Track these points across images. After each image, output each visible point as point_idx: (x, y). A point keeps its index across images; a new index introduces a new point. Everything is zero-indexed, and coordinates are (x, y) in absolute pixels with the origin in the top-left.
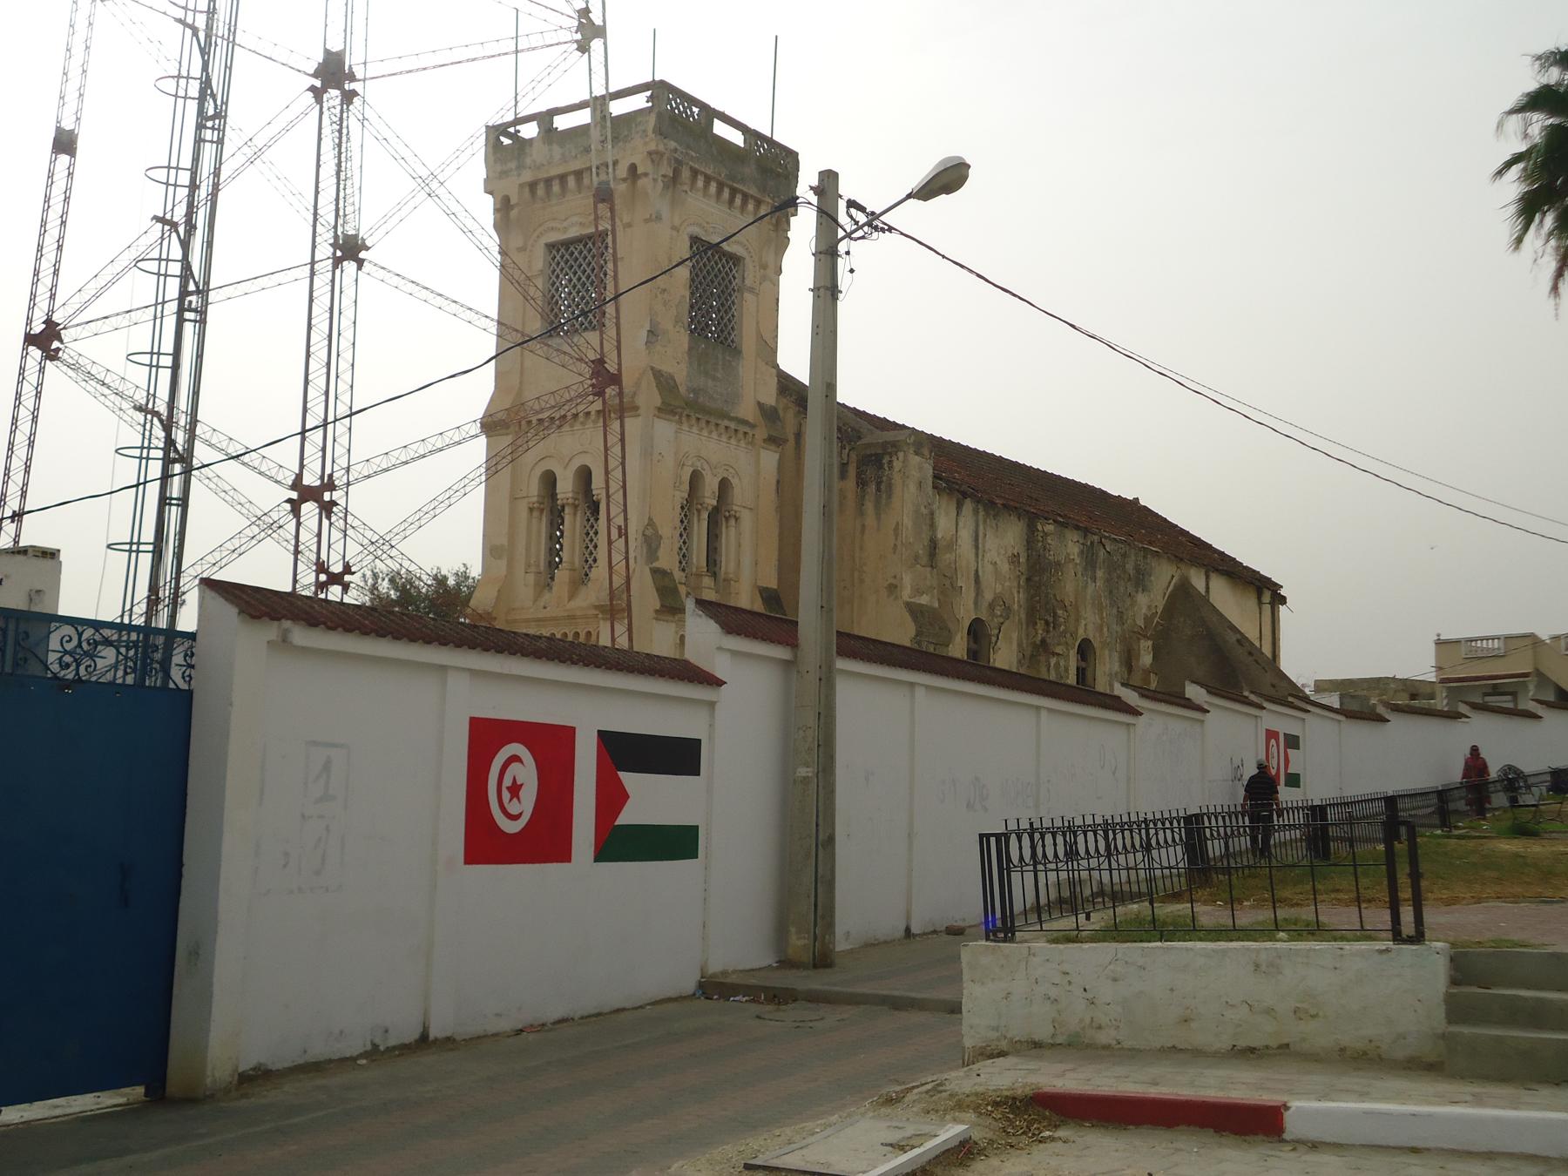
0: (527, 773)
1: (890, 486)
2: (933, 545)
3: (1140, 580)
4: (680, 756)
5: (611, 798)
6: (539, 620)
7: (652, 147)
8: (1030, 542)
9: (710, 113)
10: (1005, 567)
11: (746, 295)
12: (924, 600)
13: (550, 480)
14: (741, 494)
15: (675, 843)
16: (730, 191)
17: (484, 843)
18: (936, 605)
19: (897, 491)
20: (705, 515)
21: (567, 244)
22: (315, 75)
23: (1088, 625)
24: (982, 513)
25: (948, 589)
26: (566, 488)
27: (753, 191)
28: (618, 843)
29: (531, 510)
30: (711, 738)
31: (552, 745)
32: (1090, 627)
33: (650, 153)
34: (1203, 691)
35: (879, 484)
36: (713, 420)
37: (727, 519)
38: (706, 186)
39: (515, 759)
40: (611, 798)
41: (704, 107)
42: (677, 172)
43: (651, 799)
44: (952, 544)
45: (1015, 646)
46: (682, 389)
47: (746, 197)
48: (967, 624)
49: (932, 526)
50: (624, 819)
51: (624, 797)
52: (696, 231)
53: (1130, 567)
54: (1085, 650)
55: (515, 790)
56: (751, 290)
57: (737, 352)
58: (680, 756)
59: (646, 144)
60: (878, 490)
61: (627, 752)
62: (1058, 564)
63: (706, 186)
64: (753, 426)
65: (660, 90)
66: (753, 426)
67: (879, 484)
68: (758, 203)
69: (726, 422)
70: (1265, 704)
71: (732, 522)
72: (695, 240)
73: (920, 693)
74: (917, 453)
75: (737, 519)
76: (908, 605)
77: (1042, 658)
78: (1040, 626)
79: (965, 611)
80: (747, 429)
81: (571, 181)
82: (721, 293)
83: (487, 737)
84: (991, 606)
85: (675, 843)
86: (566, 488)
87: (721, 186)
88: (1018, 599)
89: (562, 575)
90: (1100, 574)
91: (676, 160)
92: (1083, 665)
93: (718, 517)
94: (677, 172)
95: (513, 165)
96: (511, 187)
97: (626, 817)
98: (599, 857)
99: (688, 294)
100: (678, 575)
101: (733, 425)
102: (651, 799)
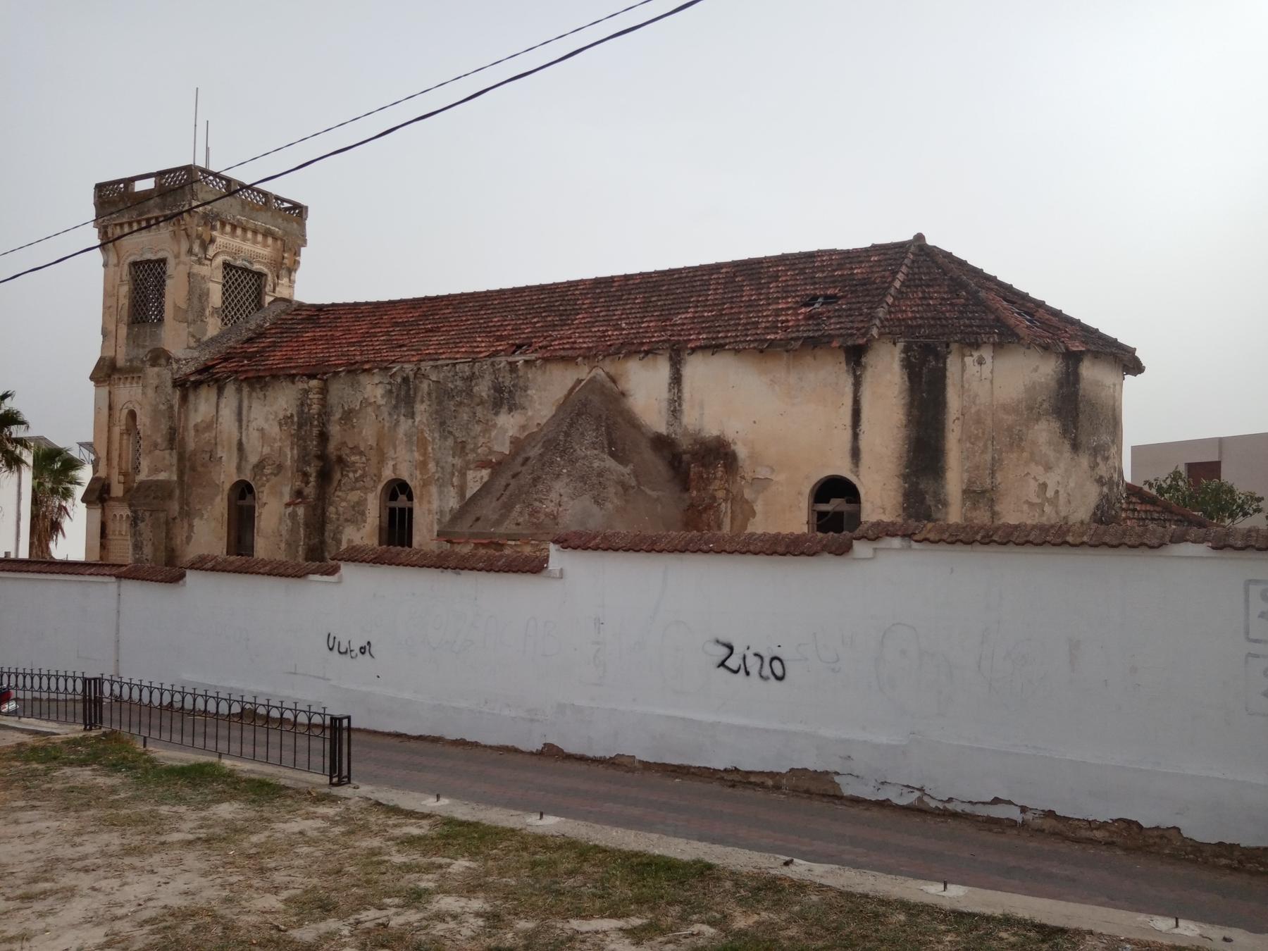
10: (274, 430)
12: (162, 476)
79: (227, 474)
90: (420, 408)
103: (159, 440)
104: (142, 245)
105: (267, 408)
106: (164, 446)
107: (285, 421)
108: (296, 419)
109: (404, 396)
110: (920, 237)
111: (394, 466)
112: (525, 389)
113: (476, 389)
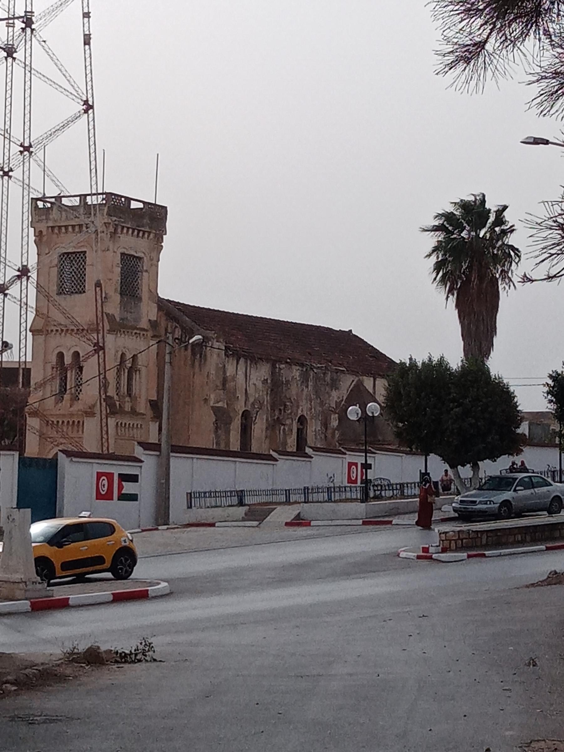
0: (106, 482)
1: (205, 355)
2: (225, 381)
3: (334, 385)
4: (134, 478)
5: (120, 487)
6: (57, 415)
7: (106, 221)
8: (273, 373)
9: (129, 200)
10: (260, 385)
11: (144, 274)
12: (220, 404)
13: (61, 356)
14: (142, 360)
15: (133, 498)
16: (138, 231)
17: (99, 496)
18: (226, 406)
19: (209, 359)
20: (126, 371)
21: (68, 254)
22: (19, 270)
23: (303, 409)
24: (249, 362)
25: (232, 396)
26: (68, 360)
27: (147, 229)
28: (124, 497)
29: (53, 368)
30: (141, 474)
31: (110, 476)
32: (305, 410)
33: (105, 223)
34: (311, 450)
35: (201, 354)
36: (130, 331)
37: (136, 371)
38: (128, 231)
39: (104, 480)
40: (120, 487)
41: (126, 198)
42: (116, 230)
43: (129, 488)
44: (234, 378)
45: (265, 421)
46: (118, 319)
47: (144, 232)
48: (241, 413)
49: (225, 372)
50: (123, 492)
51: (123, 488)
52: (123, 250)
53: (328, 378)
54: (302, 420)
55: (104, 485)
56: (146, 271)
57: (140, 299)
58: (134, 478)
59: (104, 219)
60: (201, 357)
61: (124, 478)
62: (288, 382)
63: (128, 231)
64: (147, 331)
65: (109, 196)
66: (147, 331)
67: (201, 354)
68: (149, 233)
69: (135, 331)
70: (347, 453)
71: (138, 372)
72: (122, 254)
73: (195, 460)
74: (217, 341)
75: (139, 371)
76: (212, 407)
77: (277, 427)
78: (277, 413)
79: (240, 407)
80: (144, 333)
81: (70, 229)
82: (134, 274)
83: (99, 475)
84: (253, 404)
85: (133, 498)
86: (68, 360)
87: (134, 230)
88: (267, 399)
89: (67, 397)
90: (310, 384)
91: (115, 224)
92: (301, 427)
93: (133, 370)
94: (116, 230)
95: (44, 217)
96: (42, 226)
97: (123, 492)
98: (119, 500)
99: (119, 279)
100: (116, 397)
101: (138, 332)
102: (129, 488)
103: (219, 384)
104: (69, 243)
105: (257, 374)
106: (221, 388)
107: (265, 381)
108: (269, 381)
109: (305, 378)
110: (351, 331)
111: (302, 409)
112: (340, 381)
113: (326, 378)
